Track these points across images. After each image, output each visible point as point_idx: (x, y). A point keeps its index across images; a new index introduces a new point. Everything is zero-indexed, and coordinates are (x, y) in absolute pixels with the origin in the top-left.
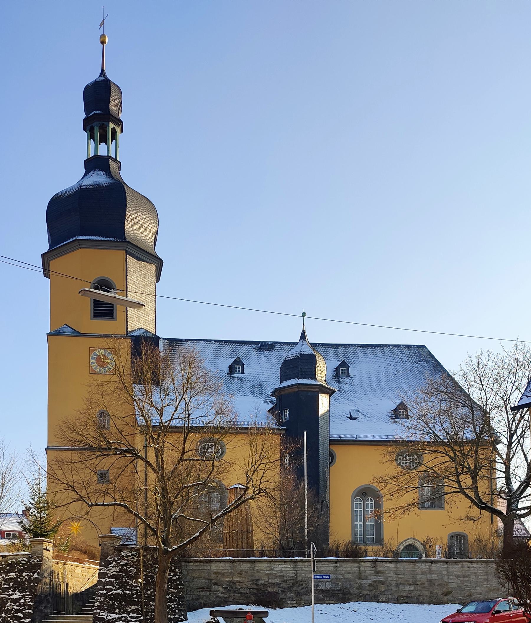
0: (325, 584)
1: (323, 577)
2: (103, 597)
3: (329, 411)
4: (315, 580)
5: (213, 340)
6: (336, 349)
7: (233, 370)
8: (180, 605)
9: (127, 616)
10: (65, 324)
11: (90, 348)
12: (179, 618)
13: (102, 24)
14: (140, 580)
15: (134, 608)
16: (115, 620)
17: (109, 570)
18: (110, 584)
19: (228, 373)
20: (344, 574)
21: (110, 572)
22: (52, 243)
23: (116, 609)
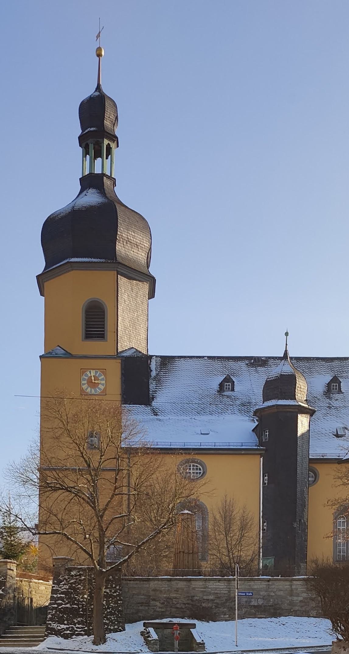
0: (257, 600)
1: (246, 594)
2: (54, 611)
3: (309, 431)
4: (239, 596)
5: (206, 357)
6: (330, 363)
7: (223, 388)
8: (119, 617)
9: (74, 627)
10: (58, 346)
11: (81, 369)
12: (118, 628)
13: (98, 36)
14: (86, 596)
15: (80, 620)
16: (63, 630)
17: (60, 587)
18: (60, 599)
19: (218, 391)
20: (276, 592)
21: (61, 589)
22: (49, 261)
23: (64, 621)
